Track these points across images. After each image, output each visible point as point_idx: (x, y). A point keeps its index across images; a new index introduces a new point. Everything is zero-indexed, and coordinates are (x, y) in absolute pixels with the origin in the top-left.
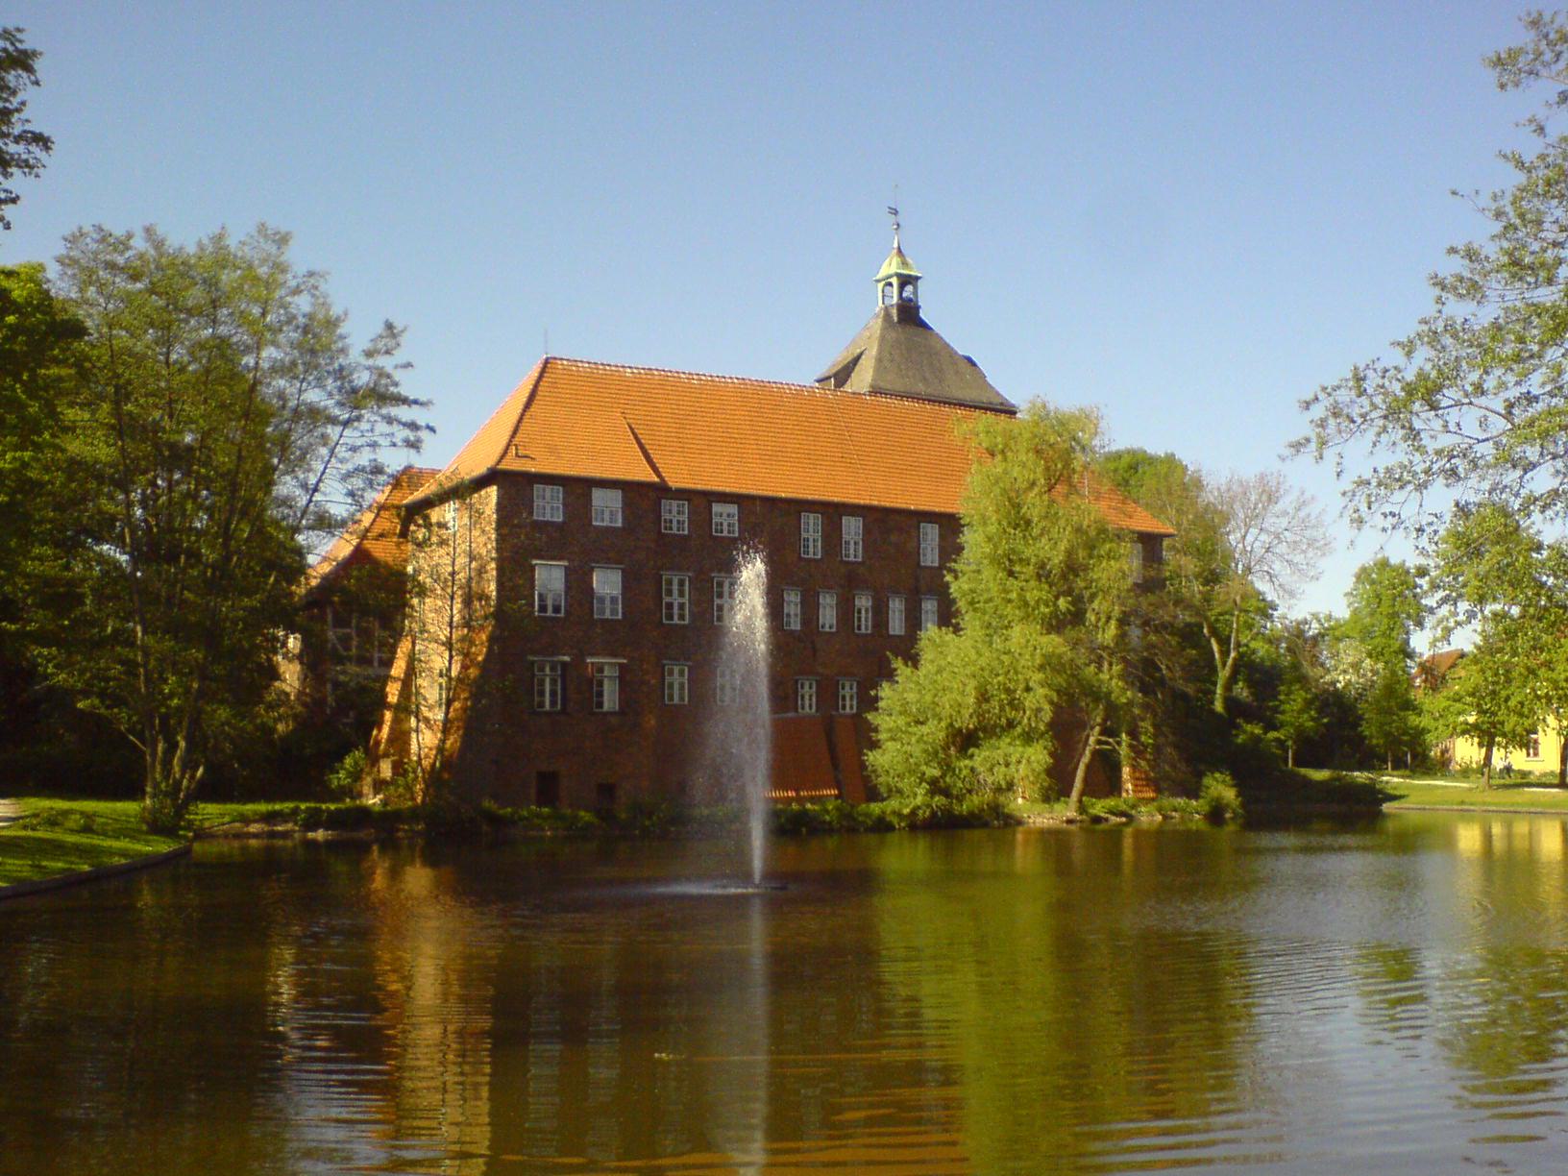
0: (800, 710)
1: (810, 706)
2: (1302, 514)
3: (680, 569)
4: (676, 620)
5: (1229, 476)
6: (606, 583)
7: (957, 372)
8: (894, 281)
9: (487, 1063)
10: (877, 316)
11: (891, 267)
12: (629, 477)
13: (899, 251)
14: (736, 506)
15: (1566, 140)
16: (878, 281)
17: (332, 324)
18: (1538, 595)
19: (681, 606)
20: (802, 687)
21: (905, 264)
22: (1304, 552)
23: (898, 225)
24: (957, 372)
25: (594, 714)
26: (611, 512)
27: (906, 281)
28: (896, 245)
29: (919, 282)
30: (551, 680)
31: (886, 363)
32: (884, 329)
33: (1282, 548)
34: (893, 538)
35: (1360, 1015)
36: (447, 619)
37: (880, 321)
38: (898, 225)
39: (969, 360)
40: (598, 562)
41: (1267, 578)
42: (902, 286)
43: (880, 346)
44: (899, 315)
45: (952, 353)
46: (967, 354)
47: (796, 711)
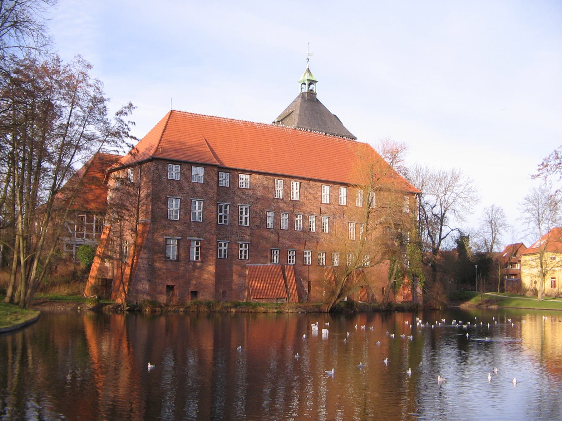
0: (272, 262)
2: (468, 186)
3: (225, 201)
4: (223, 223)
5: (440, 169)
6: (197, 208)
7: (331, 122)
8: (307, 83)
16: (299, 82)
17: (102, 100)
19: (225, 217)
20: (290, 254)
22: (468, 202)
24: (331, 122)
25: (317, 266)
26: (199, 176)
27: (311, 82)
30: (196, 248)
31: (303, 117)
32: (302, 102)
33: (459, 200)
34: (311, 191)
35: (424, 410)
36: (516, 250)
37: (300, 99)
38: (309, 60)
39: (335, 116)
40: (193, 198)
41: (453, 212)
42: (310, 84)
43: (301, 109)
45: (329, 114)
46: (334, 114)
47: (271, 262)
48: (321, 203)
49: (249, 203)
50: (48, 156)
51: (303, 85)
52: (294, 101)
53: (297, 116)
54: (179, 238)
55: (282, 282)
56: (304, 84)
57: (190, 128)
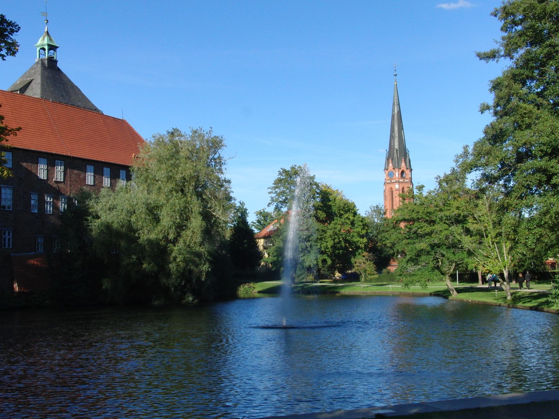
1: (9, 244)
9: (489, 286)
10: (37, 63)
11: (43, 41)
12: (112, 161)
13: (48, 33)
14: (109, 169)
15: (557, 213)
18: (523, 149)
21: (50, 40)
23: (48, 21)
27: (52, 48)
28: (46, 30)
29: (57, 49)
38: (48, 21)
44: (48, 63)
48: (94, 185)
49: (12, 185)
50: (200, 159)
51: (41, 50)
52: (32, 68)
53: (39, 86)
54: (13, 229)
55: (504, 307)
56: (44, 49)
57: (17, 106)
